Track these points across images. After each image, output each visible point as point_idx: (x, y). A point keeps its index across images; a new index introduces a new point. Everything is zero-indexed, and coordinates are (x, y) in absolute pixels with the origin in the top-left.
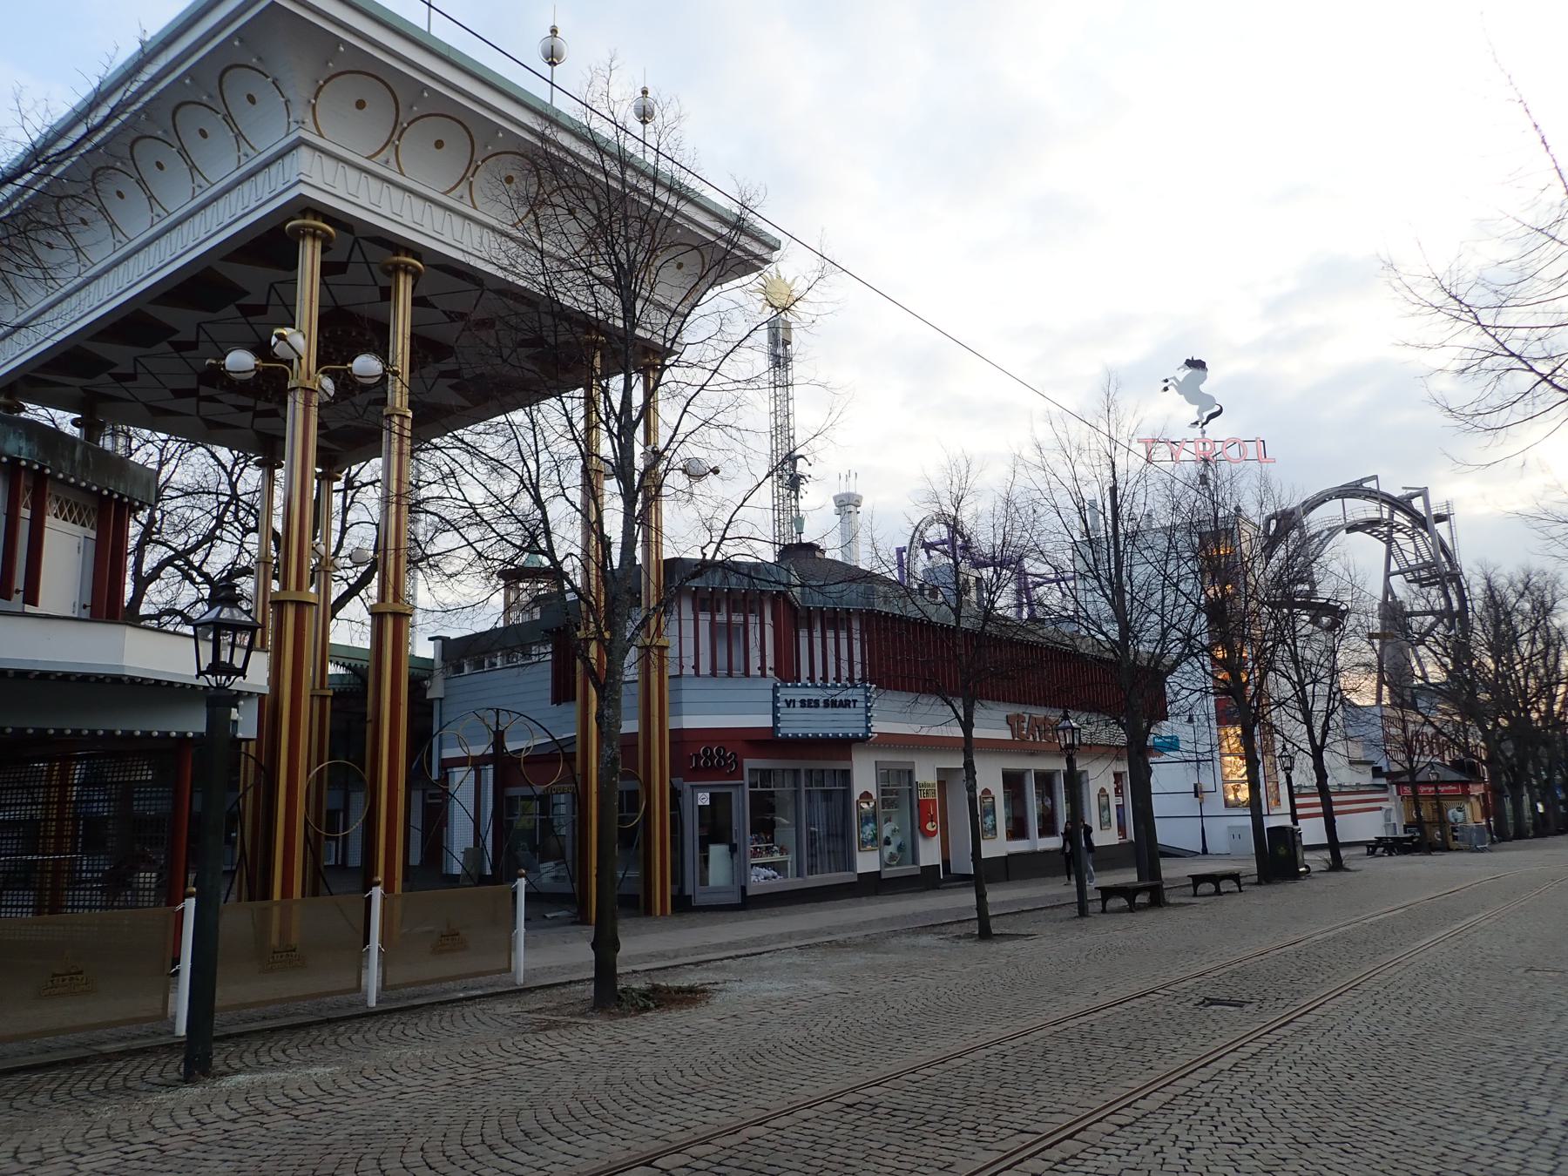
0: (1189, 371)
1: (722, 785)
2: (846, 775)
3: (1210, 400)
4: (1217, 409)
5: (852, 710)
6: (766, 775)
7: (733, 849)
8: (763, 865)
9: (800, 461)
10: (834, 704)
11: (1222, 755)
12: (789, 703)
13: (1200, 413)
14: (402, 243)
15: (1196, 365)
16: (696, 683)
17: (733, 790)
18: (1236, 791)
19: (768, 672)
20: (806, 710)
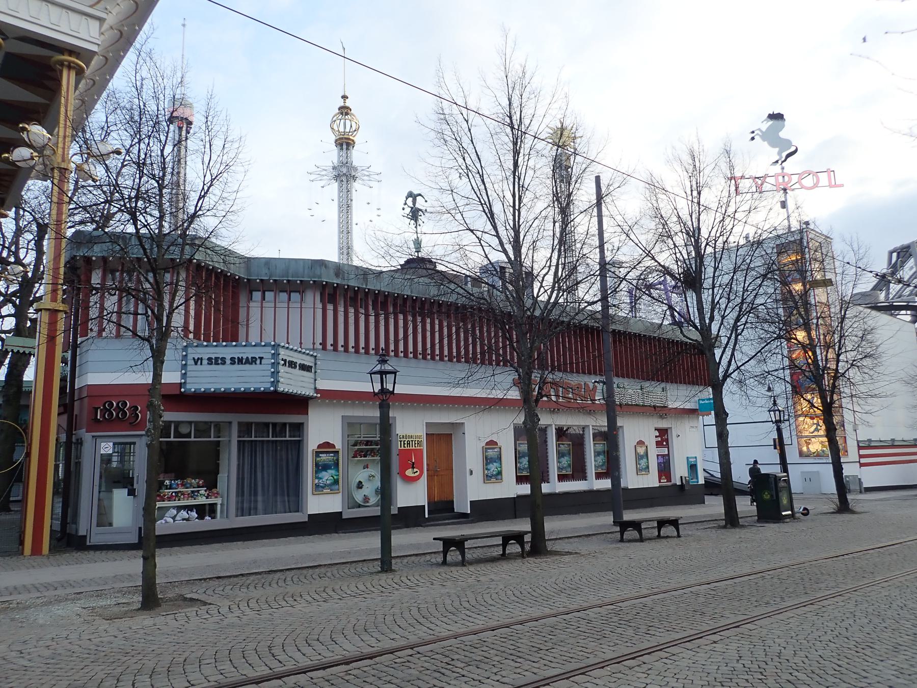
0: (771, 122)
1: (125, 435)
2: (299, 428)
3: (788, 143)
4: (793, 149)
9: (419, 198)
10: (240, 361)
11: (797, 417)
13: (780, 153)
14: (63, 46)
15: (777, 117)
18: (808, 444)
20: (214, 367)
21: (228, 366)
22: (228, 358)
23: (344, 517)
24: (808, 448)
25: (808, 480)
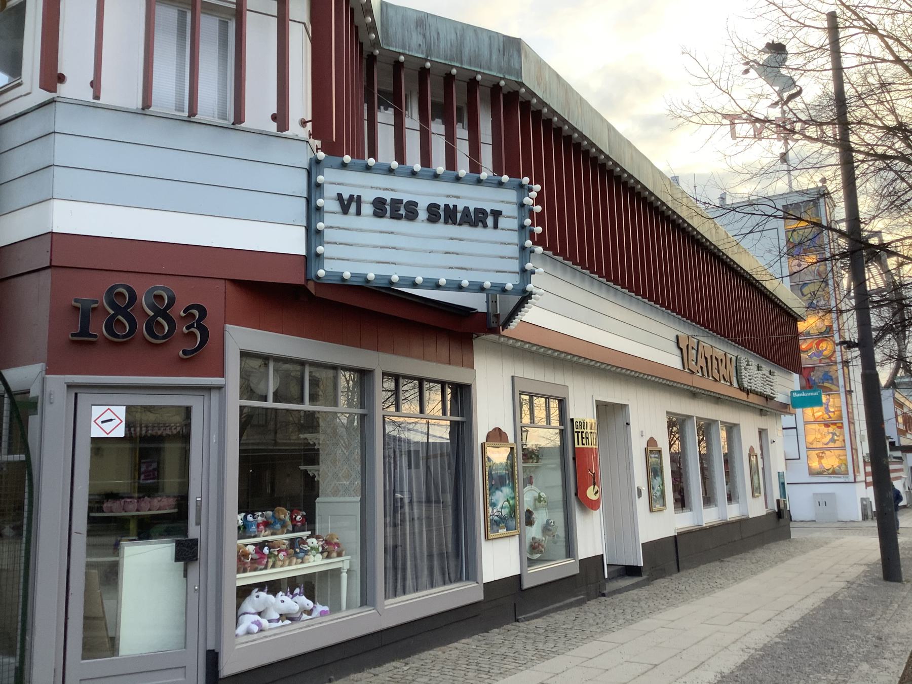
1: (164, 390)
5: (487, 233)
6: (296, 376)
7: (187, 553)
8: (273, 587)
10: (450, 215)
12: (348, 204)
13: (780, 94)
16: (96, 124)
17: (196, 403)
19: (295, 129)
20: (386, 223)
21: (421, 226)
22: (423, 205)
23: (526, 585)
24: (820, 463)
25: (822, 504)
